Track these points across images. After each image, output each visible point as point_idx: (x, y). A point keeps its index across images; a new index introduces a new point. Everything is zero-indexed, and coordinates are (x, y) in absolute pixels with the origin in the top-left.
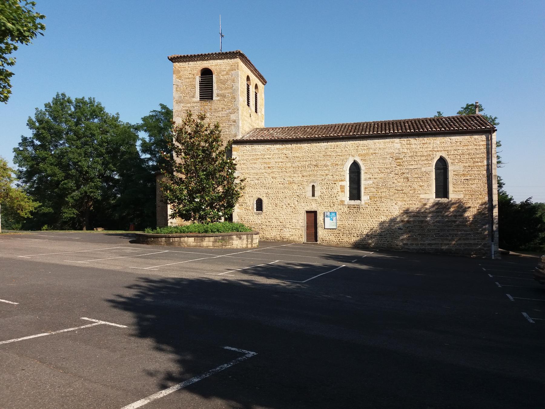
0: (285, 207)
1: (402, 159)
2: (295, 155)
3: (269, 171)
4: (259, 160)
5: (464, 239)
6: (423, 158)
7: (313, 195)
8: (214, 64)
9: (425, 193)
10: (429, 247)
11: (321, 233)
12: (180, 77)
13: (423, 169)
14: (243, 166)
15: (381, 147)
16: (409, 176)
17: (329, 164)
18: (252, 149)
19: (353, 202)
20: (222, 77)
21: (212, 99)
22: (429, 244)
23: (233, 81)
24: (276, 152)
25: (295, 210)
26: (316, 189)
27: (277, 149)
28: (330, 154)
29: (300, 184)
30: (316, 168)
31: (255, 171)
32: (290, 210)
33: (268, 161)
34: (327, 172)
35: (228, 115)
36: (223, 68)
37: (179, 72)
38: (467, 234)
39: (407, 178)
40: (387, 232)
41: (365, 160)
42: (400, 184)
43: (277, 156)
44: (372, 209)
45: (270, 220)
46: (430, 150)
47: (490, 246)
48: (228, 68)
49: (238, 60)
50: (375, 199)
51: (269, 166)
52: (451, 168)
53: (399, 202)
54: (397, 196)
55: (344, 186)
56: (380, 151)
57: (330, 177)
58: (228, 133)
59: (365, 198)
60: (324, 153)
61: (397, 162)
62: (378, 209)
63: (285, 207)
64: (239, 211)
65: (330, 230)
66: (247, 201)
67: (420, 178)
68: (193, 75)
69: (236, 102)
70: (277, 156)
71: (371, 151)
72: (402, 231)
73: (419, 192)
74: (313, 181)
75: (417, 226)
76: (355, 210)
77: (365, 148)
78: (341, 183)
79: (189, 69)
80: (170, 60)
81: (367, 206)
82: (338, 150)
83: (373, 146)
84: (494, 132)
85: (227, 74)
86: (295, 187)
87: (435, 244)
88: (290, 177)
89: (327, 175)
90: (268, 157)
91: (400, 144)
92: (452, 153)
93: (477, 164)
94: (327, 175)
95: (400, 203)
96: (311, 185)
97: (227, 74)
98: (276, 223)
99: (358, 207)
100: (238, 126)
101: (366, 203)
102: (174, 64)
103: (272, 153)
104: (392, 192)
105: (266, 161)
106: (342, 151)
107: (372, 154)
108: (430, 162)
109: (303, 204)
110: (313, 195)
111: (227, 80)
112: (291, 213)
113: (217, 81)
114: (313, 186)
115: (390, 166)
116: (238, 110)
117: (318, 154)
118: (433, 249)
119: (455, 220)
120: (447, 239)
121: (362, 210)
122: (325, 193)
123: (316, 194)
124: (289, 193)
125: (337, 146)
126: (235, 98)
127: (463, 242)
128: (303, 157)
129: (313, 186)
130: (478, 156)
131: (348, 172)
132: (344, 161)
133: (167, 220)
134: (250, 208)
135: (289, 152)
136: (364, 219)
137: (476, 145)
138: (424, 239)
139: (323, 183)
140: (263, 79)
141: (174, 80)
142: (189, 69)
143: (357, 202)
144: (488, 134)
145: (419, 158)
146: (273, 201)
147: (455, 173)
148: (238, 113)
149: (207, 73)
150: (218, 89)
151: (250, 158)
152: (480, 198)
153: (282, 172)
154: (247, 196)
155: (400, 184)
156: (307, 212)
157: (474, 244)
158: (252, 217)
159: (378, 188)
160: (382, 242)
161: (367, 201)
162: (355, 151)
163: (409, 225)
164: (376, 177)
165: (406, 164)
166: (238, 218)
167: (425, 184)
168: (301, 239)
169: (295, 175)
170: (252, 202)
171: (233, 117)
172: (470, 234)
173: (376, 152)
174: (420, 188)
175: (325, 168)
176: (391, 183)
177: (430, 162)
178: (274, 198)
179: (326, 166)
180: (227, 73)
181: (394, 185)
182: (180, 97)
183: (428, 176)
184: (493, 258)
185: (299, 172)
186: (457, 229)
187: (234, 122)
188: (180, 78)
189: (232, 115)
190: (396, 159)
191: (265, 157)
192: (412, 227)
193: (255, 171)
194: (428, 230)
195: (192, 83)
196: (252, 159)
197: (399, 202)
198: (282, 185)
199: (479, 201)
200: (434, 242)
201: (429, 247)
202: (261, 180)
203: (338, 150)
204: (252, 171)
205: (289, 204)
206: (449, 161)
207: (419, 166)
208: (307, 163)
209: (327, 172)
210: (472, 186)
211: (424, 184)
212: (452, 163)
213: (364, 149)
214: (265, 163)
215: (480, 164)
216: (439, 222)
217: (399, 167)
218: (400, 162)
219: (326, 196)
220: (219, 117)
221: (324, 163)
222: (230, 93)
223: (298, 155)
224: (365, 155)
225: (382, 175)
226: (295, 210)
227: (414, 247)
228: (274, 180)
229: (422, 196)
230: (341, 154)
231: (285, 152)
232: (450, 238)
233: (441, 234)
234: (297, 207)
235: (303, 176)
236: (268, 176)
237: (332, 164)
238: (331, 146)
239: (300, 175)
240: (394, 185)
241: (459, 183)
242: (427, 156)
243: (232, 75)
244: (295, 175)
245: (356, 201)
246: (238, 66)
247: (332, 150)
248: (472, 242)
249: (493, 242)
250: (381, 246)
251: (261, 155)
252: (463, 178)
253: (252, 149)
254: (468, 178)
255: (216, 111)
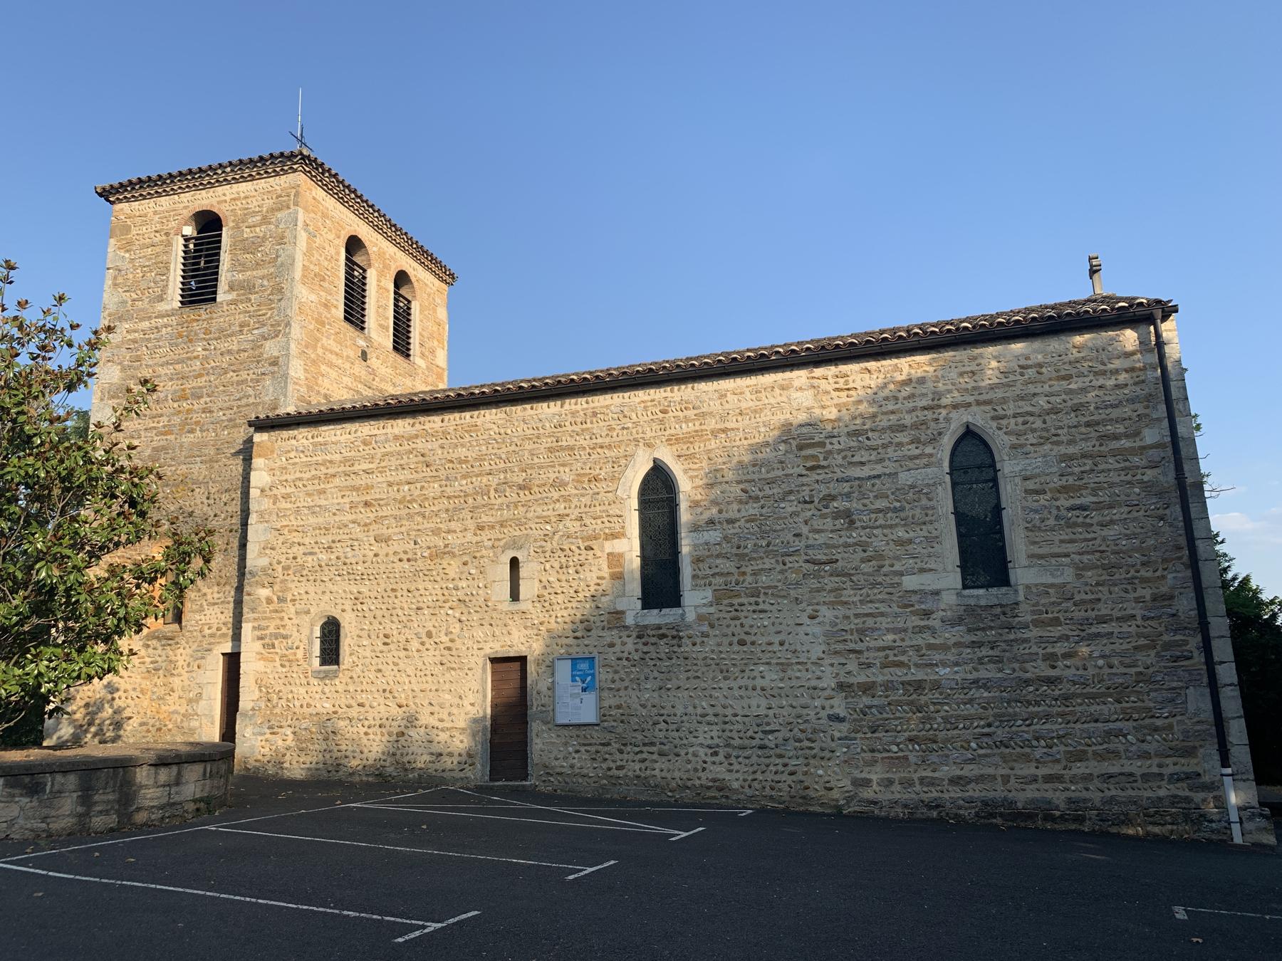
0: (415, 645)
1: (822, 444)
2: (455, 456)
3: (367, 515)
4: (337, 481)
5: (1100, 757)
6: (902, 437)
7: (515, 596)
8: (228, 198)
9: (922, 571)
10: (955, 793)
11: (542, 744)
12: (130, 243)
13: (905, 478)
14: (283, 504)
15: (744, 405)
16: (855, 505)
17: (567, 476)
18: (315, 445)
19: (654, 617)
20: (247, 233)
21: (214, 299)
22: (955, 781)
23: (281, 240)
24: (392, 447)
25: (450, 657)
26: (523, 572)
27: (396, 438)
28: (571, 442)
29: (471, 556)
30: (525, 496)
31: (321, 520)
32: (431, 656)
33: (362, 481)
34: (560, 507)
35: (256, 346)
36: (253, 205)
37: (127, 229)
38: (1109, 733)
39: (847, 514)
40: (785, 733)
41: (690, 457)
42: (821, 538)
43: (394, 462)
44: (726, 641)
45: (362, 698)
46: (924, 403)
47: (1214, 787)
48: (269, 203)
49: (299, 179)
50: (736, 601)
51: (368, 498)
52: (1009, 467)
53: (824, 610)
54: (813, 583)
55: (621, 555)
56: (744, 422)
57: (572, 526)
58: (251, 400)
59: (694, 598)
60: (547, 442)
61: (807, 458)
62: (748, 639)
63: (415, 645)
64: (260, 666)
65: (574, 732)
66: (290, 629)
67: (895, 510)
68: (167, 234)
69: (283, 303)
70: (394, 462)
71: (712, 424)
72: (844, 727)
73: (897, 567)
74: (514, 544)
75: (899, 703)
76: (664, 648)
77: (691, 413)
78: (609, 546)
79: (156, 218)
80: (100, 195)
81: (705, 628)
82: (598, 427)
83: (715, 406)
84: (1165, 318)
85: (265, 221)
86: (453, 567)
87: (980, 779)
88: (436, 532)
89: (561, 517)
90: (365, 466)
91: (811, 392)
92: (1011, 409)
93: (1114, 445)
94: (561, 517)
95: (827, 613)
96: (506, 559)
97: (265, 221)
98: (382, 708)
99: (673, 635)
100: (285, 376)
101: (700, 618)
102: (118, 207)
103: (380, 452)
104: (797, 571)
105: (357, 481)
106: (611, 429)
107: (714, 433)
108: (929, 450)
109: (479, 633)
110: (515, 596)
111: (264, 239)
112: (438, 670)
113: (234, 245)
114: (514, 563)
115: (780, 473)
116: (288, 324)
117: (528, 446)
118: (970, 801)
119: (1052, 673)
120: (1027, 758)
121: (687, 648)
122: (556, 585)
123: (526, 589)
124: (430, 591)
125: (595, 414)
126: (280, 290)
127: (1093, 767)
128: (480, 459)
129: (514, 563)
130: (1115, 413)
131: (634, 503)
132: (620, 465)
133: (43, 721)
134: (300, 654)
135: (436, 445)
136: (695, 683)
137: (1104, 373)
138: (934, 758)
139: (548, 546)
140: (433, 260)
141: (110, 255)
142: (156, 218)
143: (665, 616)
144: (1142, 328)
145: (886, 437)
146: (376, 626)
147: (1031, 485)
148: (287, 335)
149: (209, 223)
150: (233, 269)
151: (308, 475)
152: (1144, 580)
153: (410, 517)
154: (292, 610)
155: (821, 538)
156: (494, 661)
157: (1146, 777)
158: (302, 690)
159: (741, 557)
160: (770, 776)
161: (704, 610)
162: (655, 426)
163: (866, 700)
164: (731, 515)
165: (840, 461)
166: (257, 694)
167: (918, 534)
168: (469, 773)
169: (453, 525)
170: (305, 632)
171: (271, 349)
172: (1120, 733)
173: (729, 425)
174: (900, 551)
175: (556, 495)
176: (790, 537)
177: (929, 450)
178: (379, 614)
179: (559, 484)
180: (264, 218)
181: (799, 544)
182: (124, 302)
183: (924, 502)
184: (1238, 840)
185: (466, 514)
186: (1061, 715)
187: (275, 363)
188: (127, 246)
189: (268, 344)
190: (800, 448)
191: (356, 468)
192: (881, 709)
193: (321, 520)
194: (946, 720)
195: (160, 259)
196: (314, 478)
197: (824, 610)
198: (406, 565)
199: (1140, 592)
200: (969, 771)
201: (955, 793)
202: (339, 550)
203: (598, 427)
204: (312, 520)
205: (429, 635)
206: (1000, 441)
207: (890, 467)
208: (494, 481)
209: (560, 507)
210: (1106, 532)
211: (912, 534)
212: (1013, 447)
213: (687, 420)
214: (355, 489)
215: (1125, 443)
216: (985, 687)
217: (814, 476)
218: (814, 457)
219: (560, 598)
220: (229, 352)
221: (553, 476)
222: (269, 277)
223: (462, 452)
224: (689, 439)
225: (753, 509)
226: (450, 657)
227: (897, 792)
228: (382, 549)
229: (910, 582)
230: (607, 440)
231: (420, 445)
232: (1038, 753)
233: (1001, 734)
234: (458, 644)
235: (481, 528)
236: (360, 536)
237: (579, 478)
238: (574, 414)
239: (471, 524)
240: (799, 544)
241: (1051, 522)
242: (915, 426)
243: (302, 230)
244: (453, 525)
245: (665, 611)
246: (297, 194)
247: (577, 428)
248: (1136, 767)
249: (1225, 764)
250: (768, 792)
251: (345, 461)
252: (1064, 502)
253: (315, 445)
254: (1087, 499)
255: (223, 334)
